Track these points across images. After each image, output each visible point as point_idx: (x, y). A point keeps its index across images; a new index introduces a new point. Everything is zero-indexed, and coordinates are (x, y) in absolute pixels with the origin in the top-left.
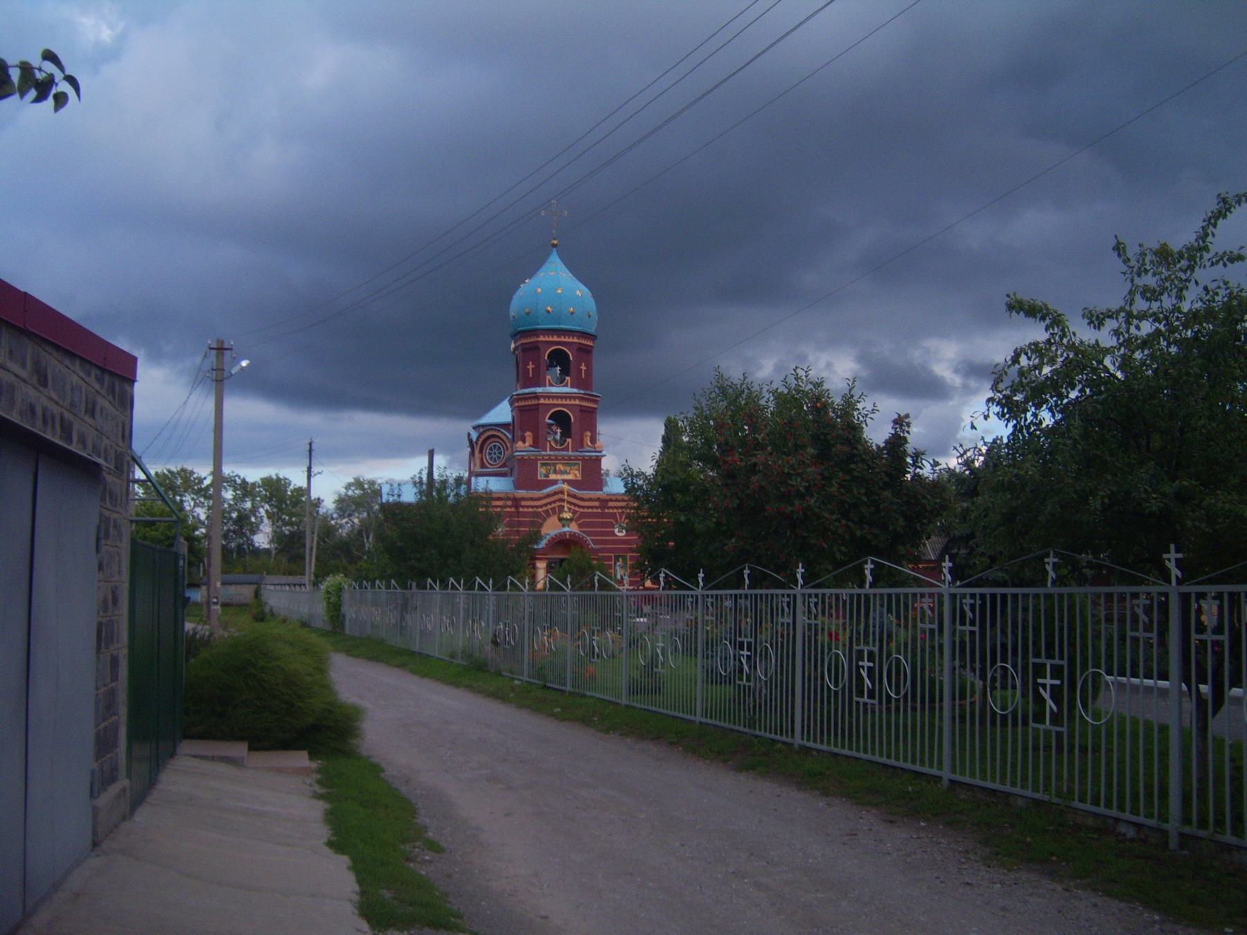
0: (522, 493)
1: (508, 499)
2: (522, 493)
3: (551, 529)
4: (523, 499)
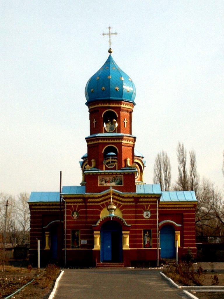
0: (88, 194)
1: (80, 198)
2: (88, 194)
3: (104, 214)
4: (89, 198)
